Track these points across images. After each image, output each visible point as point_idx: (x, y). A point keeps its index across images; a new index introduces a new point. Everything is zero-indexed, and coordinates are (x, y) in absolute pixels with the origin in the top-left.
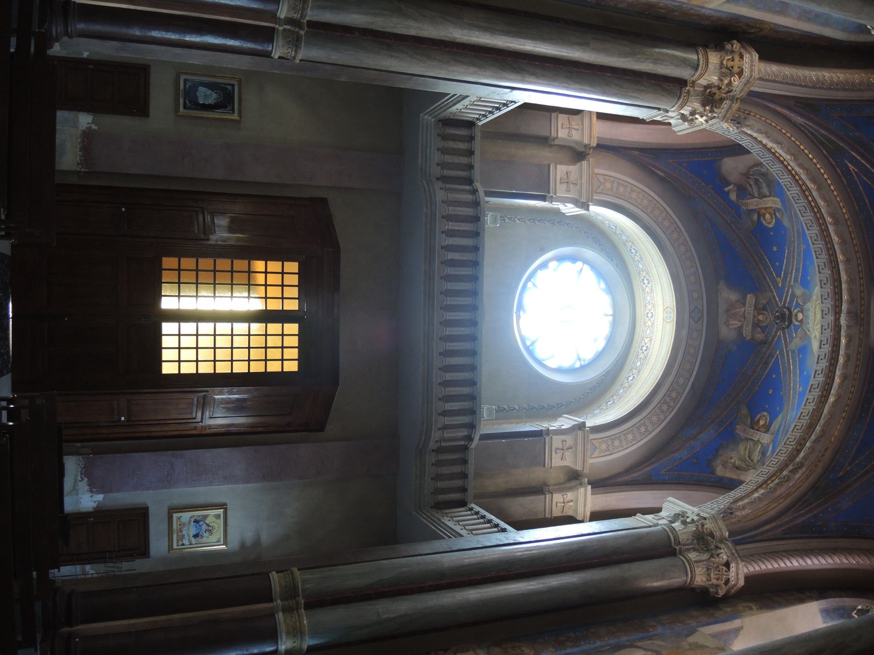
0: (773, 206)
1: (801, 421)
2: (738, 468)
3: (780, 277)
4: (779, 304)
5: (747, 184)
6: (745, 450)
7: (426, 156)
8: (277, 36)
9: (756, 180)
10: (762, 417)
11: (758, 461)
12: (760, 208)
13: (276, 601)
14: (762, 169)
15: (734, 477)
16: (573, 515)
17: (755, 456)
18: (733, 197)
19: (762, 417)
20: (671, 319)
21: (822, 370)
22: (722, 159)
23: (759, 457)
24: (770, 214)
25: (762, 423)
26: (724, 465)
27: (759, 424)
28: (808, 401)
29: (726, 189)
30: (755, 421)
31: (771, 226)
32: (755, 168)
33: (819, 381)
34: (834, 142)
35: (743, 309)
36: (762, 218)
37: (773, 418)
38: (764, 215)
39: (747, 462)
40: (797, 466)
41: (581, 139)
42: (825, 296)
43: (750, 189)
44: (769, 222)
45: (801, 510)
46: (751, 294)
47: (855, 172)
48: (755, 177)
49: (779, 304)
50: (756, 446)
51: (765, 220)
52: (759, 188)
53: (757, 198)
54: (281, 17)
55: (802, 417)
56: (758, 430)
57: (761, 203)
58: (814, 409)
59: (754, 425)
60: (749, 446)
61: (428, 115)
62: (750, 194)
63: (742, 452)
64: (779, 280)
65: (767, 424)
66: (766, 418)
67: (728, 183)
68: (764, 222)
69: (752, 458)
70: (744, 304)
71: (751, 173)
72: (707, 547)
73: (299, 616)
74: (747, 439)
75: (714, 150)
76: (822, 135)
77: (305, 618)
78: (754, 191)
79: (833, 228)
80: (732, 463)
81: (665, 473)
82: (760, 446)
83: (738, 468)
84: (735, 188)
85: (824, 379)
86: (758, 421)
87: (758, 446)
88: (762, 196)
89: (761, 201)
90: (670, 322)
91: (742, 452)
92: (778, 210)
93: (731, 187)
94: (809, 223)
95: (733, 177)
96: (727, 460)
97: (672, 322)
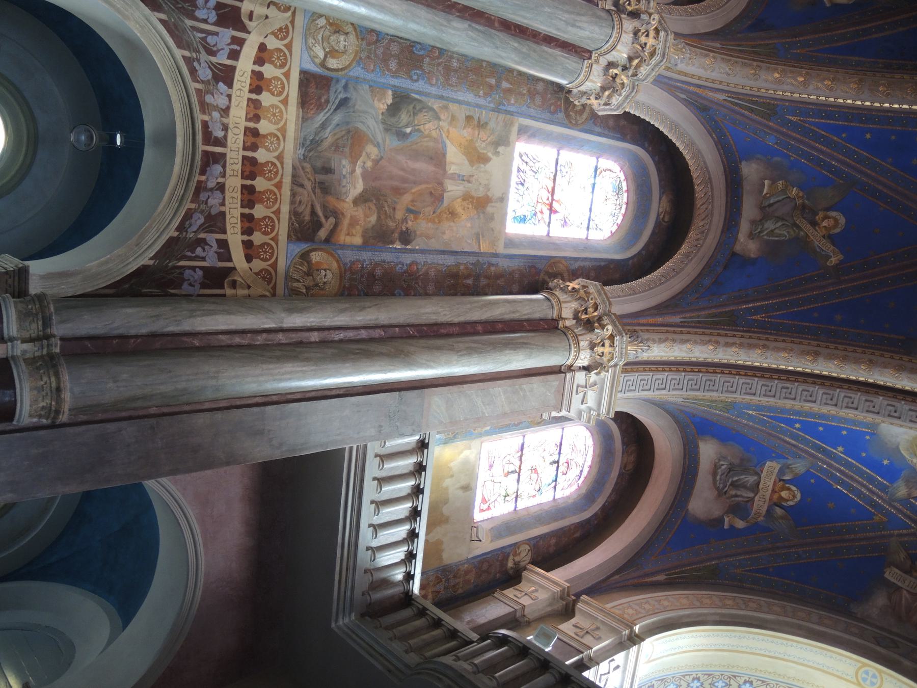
0: (773, 480)
3: (874, 515)
4: (912, 530)
5: (733, 499)
7: (381, 655)
8: (16, 364)
9: (734, 485)
12: (770, 499)
14: (723, 467)
18: (740, 524)
20: (877, 674)
22: (687, 509)
24: (783, 488)
29: (726, 527)
31: (799, 496)
32: (718, 477)
34: (721, 313)
35: (905, 592)
36: (784, 504)
38: (781, 498)
41: (550, 594)
42: (912, 416)
43: (740, 499)
44: (792, 496)
46: (885, 570)
47: (765, 317)
48: (728, 484)
49: (912, 530)
51: (788, 500)
52: (744, 486)
53: (756, 495)
54: (15, 354)
57: (764, 494)
61: (341, 616)
62: (747, 502)
64: (877, 518)
67: (720, 521)
68: (791, 503)
70: (899, 588)
71: (721, 486)
75: (671, 512)
76: (710, 316)
78: (746, 495)
79: (822, 359)
84: (731, 516)
88: (755, 488)
89: (761, 493)
90: (882, 679)
92: (781, 472)
93: (726, 519)
94: (806, 396)
95: (717, 512)
97: (883, 675)
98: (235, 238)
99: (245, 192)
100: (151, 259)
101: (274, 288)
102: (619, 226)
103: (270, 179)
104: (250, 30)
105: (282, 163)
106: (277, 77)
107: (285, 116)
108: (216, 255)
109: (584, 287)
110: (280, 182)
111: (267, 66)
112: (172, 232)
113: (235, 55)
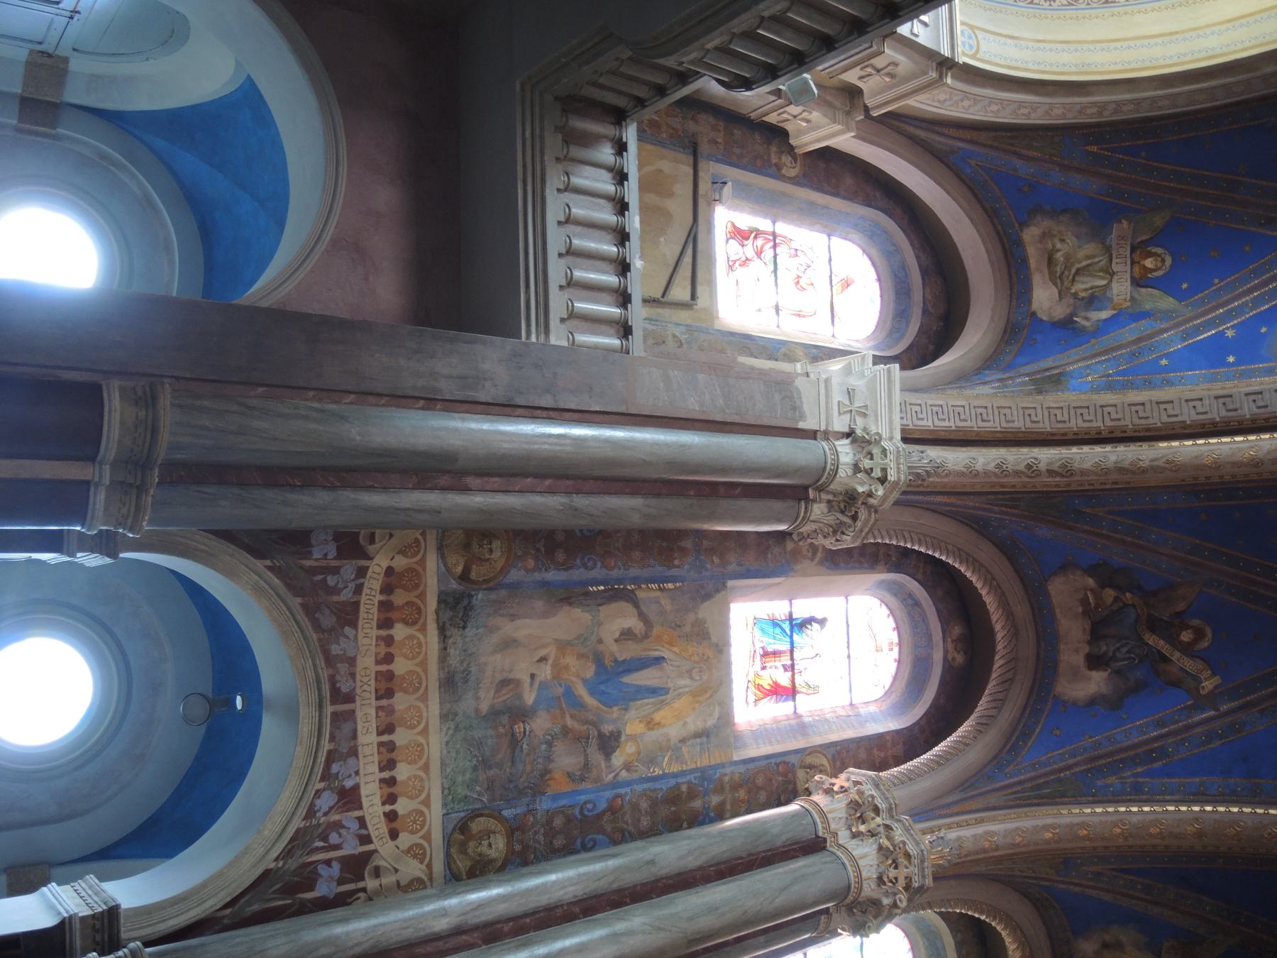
1: (1155, 407)
2: (1051, 262)
6: (1088, 257)
10: (1159, 259)
11: (1075, 295)
13: (101, 464)
15: (1033, 263)
16: (790, 133)
17: (1083, 283)
19: (1159, 259)
21: (1266, 406)
23: (1083, 294)
25: (1149, 263)
26: (1045, 236)
27: (1145, 259)
28: (1197, 403)
30: (1149, 249)
33: (1241, 408)
37: (1166, 285)
39: (1066, 273)
40: (1064, 473)
45: (996, 505)
50: (1101, 274)
55: (1163, 406)
56: (1133, 263)
58: (1186, 421)
59: (1139, 249)
60: (1097, 260)
63: (1081, 254)
65: (1149, 276)
66: (1160, 269)
69: (1077, 278)
72: (845, 507)
73: (138, 508)
74: (1108, 250)
77: (146, 518)
80: (1054, 246)
81: (973, 165)
82: (1104, 282)
83: (1051, 262)
85: (1248, 416)
86: (1149, 255)
87: (1102, 278)
91: (1081, 254)
96: (1054, 236)
98: (373, 806)
99: (383, 750)
100: (276, 860)
101: (429, 866)
102: (899, 661)
103: (413, 727)
104: (371, 556)
105: (429, 842)
106: (411, 671)
107: (425, 714)
108: (356, 821)
109: (856, 783)
110: (425, 660)
111: (398, 591)
112: (297, 823)
113: (359, 590)
